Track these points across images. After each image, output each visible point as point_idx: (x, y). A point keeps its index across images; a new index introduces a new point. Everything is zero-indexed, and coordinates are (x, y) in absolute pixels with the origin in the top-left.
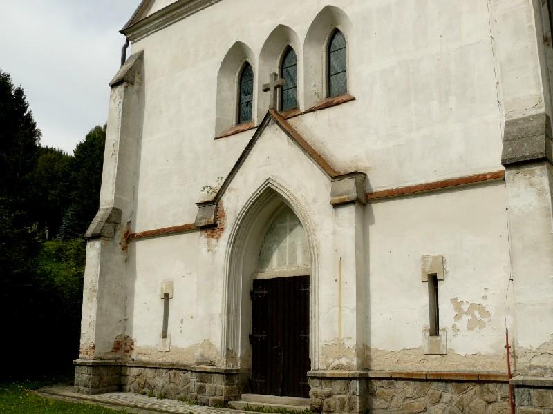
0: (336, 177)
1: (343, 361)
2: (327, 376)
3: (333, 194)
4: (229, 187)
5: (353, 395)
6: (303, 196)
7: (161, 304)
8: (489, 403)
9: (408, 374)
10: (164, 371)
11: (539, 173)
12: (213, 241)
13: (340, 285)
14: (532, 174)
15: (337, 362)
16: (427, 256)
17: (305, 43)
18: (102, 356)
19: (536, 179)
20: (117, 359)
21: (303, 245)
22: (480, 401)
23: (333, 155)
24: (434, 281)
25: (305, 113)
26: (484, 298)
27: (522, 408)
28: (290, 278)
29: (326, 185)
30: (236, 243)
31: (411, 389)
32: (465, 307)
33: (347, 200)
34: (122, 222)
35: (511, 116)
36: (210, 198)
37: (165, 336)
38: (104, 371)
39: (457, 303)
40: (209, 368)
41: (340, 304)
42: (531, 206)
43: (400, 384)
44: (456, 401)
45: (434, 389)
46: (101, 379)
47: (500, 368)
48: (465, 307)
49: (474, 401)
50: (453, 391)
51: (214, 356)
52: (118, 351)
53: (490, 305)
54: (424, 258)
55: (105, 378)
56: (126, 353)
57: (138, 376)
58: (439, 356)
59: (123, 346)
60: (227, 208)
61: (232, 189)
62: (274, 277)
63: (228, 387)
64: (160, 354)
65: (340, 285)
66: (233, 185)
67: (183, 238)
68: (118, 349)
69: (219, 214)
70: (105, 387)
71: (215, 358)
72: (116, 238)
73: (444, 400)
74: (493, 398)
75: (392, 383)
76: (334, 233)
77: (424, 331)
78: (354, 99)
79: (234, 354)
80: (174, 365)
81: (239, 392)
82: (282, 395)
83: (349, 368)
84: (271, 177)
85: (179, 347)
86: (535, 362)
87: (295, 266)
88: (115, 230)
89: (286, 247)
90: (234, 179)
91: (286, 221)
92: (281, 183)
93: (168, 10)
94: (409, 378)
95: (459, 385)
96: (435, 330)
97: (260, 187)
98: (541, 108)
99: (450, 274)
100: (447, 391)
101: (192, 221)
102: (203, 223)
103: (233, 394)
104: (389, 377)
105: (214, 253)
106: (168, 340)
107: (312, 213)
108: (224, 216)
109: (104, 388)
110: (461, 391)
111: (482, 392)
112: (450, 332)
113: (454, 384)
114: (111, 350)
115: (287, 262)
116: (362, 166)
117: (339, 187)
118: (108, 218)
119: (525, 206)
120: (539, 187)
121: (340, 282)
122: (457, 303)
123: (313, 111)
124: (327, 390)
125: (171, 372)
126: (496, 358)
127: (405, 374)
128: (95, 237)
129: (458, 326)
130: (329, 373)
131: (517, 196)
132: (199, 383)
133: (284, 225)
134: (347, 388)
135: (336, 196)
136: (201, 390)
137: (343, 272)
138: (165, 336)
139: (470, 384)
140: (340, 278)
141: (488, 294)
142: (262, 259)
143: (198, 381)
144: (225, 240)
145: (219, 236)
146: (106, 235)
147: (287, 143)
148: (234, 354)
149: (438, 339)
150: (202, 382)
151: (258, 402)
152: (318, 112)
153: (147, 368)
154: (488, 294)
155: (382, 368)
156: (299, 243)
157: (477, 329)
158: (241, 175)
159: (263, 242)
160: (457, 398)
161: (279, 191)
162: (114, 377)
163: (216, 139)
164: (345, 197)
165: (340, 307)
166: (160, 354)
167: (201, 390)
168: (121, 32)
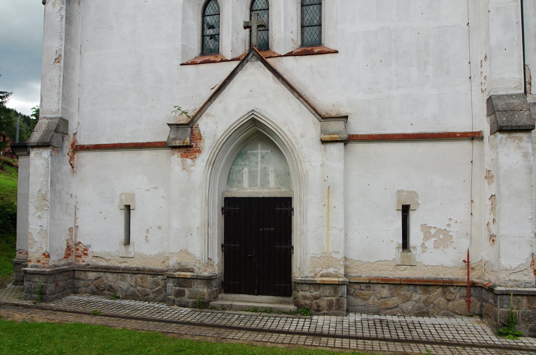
0: (324, 118)
1: (331, 270)
2: (318, 282)
3: (323, 132)
4: (206, 113)
5: (341, 297)
6: (290, 131)
7: (121, 217)
8: (449, 300)
9: (382, 280)
10: (129, 275)
12: (189, 161)
13: (328, 210)
14: (521, 139)
15: (324, 271)
16: (402, 191)
18: (56, 263)
19: (522, 144)
20: (69, 264)
21: (275, 171)
22: (443, 299)
23: (315, 98)
24: (406, 210)
26: (449, 225)
27: (503, 309)
28: (264, 199)
29: (315, 124)
30: (212, 164)
31: (385, 292)
32: (433, 231)
33: (338, 139)
34: (69, 133)
35: (497, 92)
36: (184, 120)
37: (127, 242)
38: (59, 277)
39: (425, 228)
40: (189, 274)
41: (328, 225)
42: (518, 164)
43: (378, 288)
44: (423, 299)
45: (404, 291)
46: (57, 285)
47: (460, 275)
48: (433, 231)
49: (438, 299)
50: (421, 292)
51: (192, 264)
52: (70, 257)
53: (454, 230)
54: (399, 192)
55: (61, 284)
56: (78, 258)
57: (95, 279)
58: (409, 266)
59: (74, 252)
60: (204, 132)
61: (208, 115)
62: (246, 196)
63: (209, 290)
64: (121, 260)
65: (328, 210)
66: (209, 111)
67: (146, 154)
68: (69, 255)
69: (196, 137)
70: (61, 291)
71: (194, 265)
72: (65, 148)
73: (414, 299)
74: (453, 297)
75: (370, 287)
76: (322, 165)
77: (398, 248)
78: (336, 52)
79: (212, 262)
80: (140, 270)
81: (217, 293)
82: (258, 294)
83: (337, 276)
84: (255, 109)
85: (145, 253)
86: (512, 277)
87: (268, 188)
88: (63, 140)
90: (212, 105)
91: (257, 148)
92: (266, 116)
94: (385, 282)
95: (427, 288)
96: (405, 245)
99: (421, 206)
100: (416, 292)
101: (164, 139)
102: (178, 143)
103: (213, 296)
104: (368, 282)
105: (190, 172)
106: (131, 248)
107: (300, 146)
108: (201, 139)
109: (60, 294)
110: (426, 292)
111: (444, 293)
112: (419, 250)
113: (422, 287)
114: (64, 255)
115: (259, 185)
117: (329, 127)
118: (57, 128)
120: (524, 151)
121: (328, 206)
122: (425, 228)
123: (295, 55)
124: (315, 293)
125: (137, 276)
126: (455, 269)
127: (382, 280)
128: (43, 145)
129: (427, 244)
130: (318, 279)
131: (507, 155)
132: (177, 288)
133: (255, 151)
134: (336, 293)
136: (180, 294)
137: (330, 199)
138: (127, 242)
139: (435, 287)
141: (452, 223)
142: (230, 179)
143: (175, 286)
144: (203, 161)
145: (196, 158)
146: (55, 145)
147: (271, 79)
148: (212, 262)
149: (409, 254)
150: (180, 286)
151: (248, 302)
152: (299, 57)
153: (107, 272)
154: (452, 223)
155: (359, 274)
157: (441, 248)
158: (220, 103)
159: (233, 165)
160: (424, 297)
162: (68, 281)
163: (181, 65)
164: (336, 136)
165: (328, 227)
166: (121, 260)
167: (180, 294)
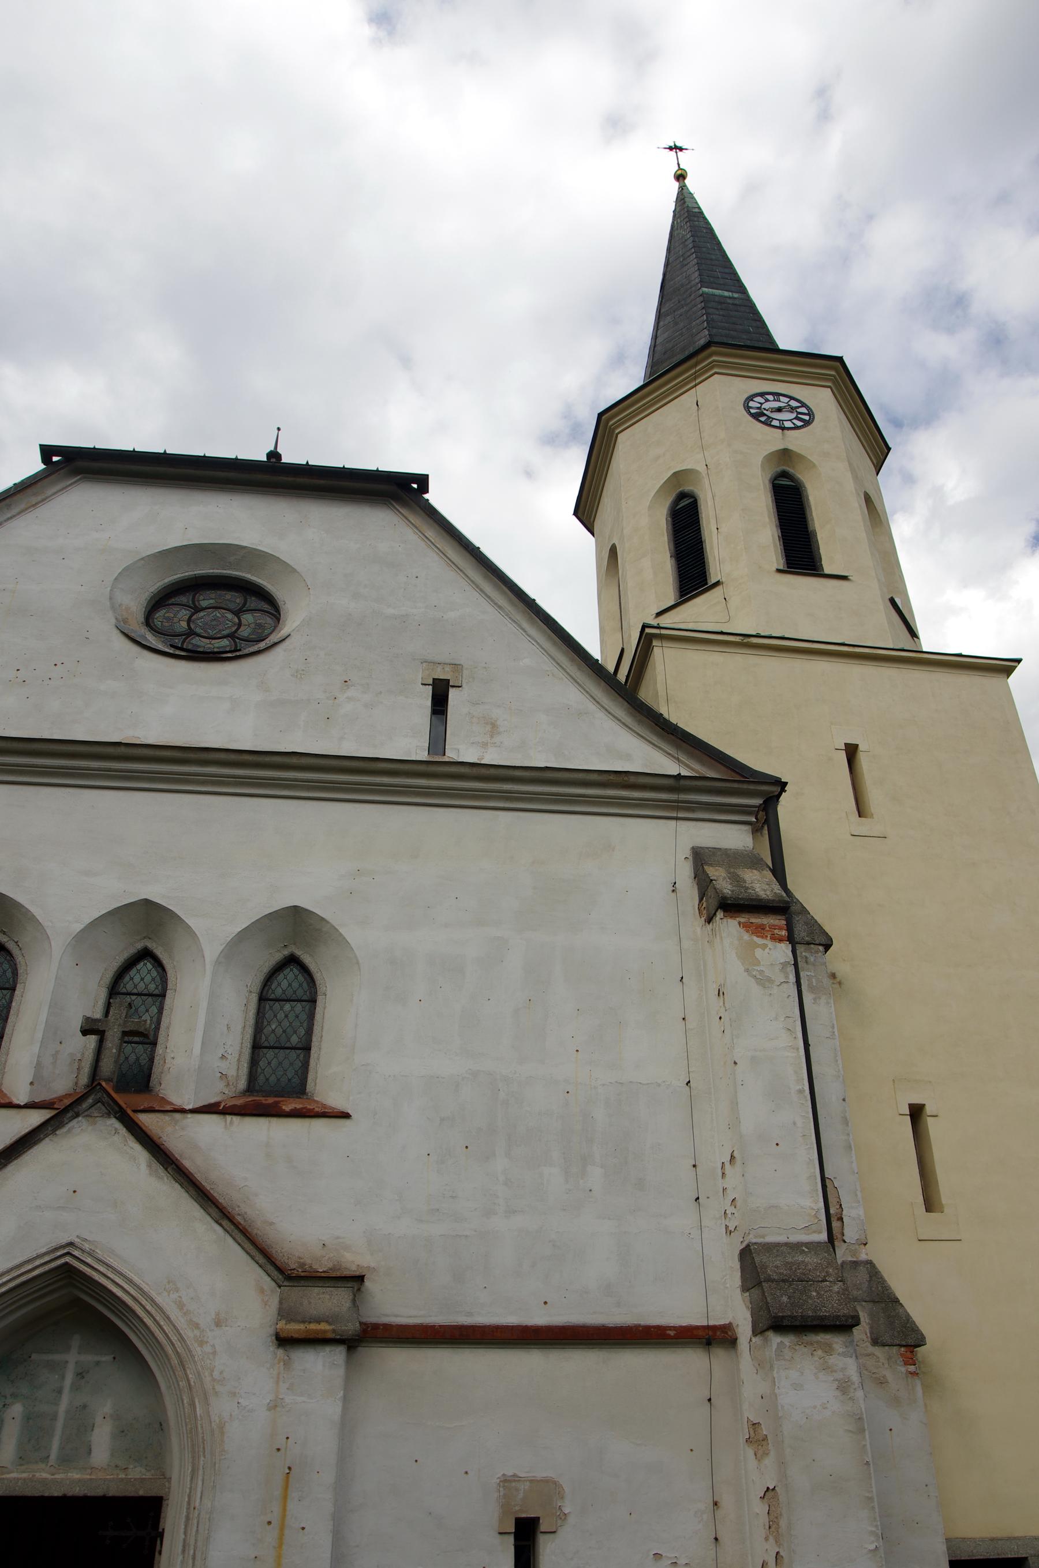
3: (285, 1313)
11: (841, 1350)
14: (828, 1349)
17: (218, 963)
25: (194, 1111)
35: (763, 1237)
54: (507, 1482)
76: (274, 1406)
89: (54, 1417)
93: (233, 757)
97: (130, 1281)
98: (820, 1232)
99: (571, 1520)
107: (208, 1349)
116: (354, 1261)
119: (815, 1407)
120: (839, 1375)
121: (282, 1528)
131: (797, 1387)
135: (290, 1320)
140: (284, 1516)
152: (236, 1119)
156: (107, 1408)
161: (96, 1276)
168: (787, 783)
